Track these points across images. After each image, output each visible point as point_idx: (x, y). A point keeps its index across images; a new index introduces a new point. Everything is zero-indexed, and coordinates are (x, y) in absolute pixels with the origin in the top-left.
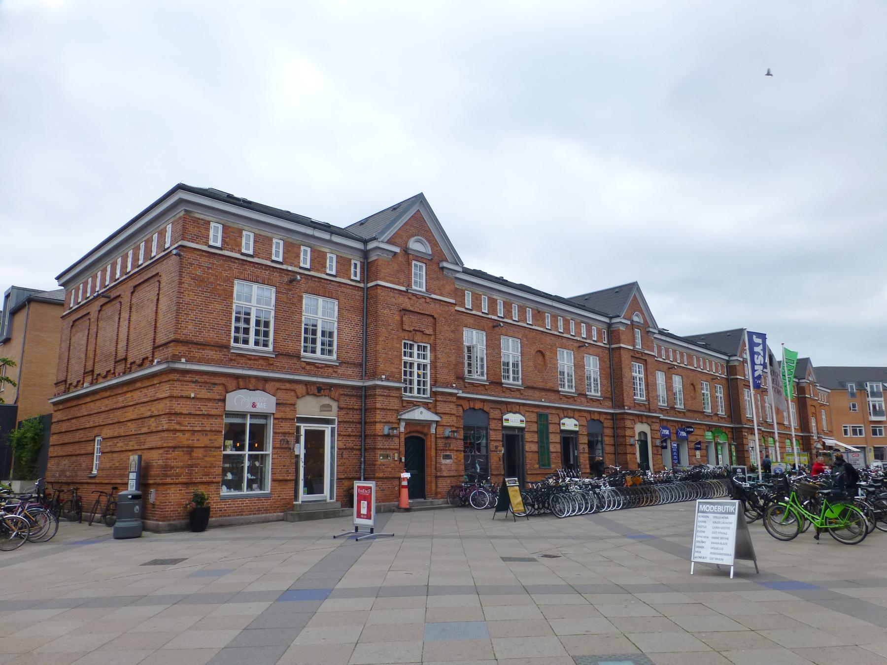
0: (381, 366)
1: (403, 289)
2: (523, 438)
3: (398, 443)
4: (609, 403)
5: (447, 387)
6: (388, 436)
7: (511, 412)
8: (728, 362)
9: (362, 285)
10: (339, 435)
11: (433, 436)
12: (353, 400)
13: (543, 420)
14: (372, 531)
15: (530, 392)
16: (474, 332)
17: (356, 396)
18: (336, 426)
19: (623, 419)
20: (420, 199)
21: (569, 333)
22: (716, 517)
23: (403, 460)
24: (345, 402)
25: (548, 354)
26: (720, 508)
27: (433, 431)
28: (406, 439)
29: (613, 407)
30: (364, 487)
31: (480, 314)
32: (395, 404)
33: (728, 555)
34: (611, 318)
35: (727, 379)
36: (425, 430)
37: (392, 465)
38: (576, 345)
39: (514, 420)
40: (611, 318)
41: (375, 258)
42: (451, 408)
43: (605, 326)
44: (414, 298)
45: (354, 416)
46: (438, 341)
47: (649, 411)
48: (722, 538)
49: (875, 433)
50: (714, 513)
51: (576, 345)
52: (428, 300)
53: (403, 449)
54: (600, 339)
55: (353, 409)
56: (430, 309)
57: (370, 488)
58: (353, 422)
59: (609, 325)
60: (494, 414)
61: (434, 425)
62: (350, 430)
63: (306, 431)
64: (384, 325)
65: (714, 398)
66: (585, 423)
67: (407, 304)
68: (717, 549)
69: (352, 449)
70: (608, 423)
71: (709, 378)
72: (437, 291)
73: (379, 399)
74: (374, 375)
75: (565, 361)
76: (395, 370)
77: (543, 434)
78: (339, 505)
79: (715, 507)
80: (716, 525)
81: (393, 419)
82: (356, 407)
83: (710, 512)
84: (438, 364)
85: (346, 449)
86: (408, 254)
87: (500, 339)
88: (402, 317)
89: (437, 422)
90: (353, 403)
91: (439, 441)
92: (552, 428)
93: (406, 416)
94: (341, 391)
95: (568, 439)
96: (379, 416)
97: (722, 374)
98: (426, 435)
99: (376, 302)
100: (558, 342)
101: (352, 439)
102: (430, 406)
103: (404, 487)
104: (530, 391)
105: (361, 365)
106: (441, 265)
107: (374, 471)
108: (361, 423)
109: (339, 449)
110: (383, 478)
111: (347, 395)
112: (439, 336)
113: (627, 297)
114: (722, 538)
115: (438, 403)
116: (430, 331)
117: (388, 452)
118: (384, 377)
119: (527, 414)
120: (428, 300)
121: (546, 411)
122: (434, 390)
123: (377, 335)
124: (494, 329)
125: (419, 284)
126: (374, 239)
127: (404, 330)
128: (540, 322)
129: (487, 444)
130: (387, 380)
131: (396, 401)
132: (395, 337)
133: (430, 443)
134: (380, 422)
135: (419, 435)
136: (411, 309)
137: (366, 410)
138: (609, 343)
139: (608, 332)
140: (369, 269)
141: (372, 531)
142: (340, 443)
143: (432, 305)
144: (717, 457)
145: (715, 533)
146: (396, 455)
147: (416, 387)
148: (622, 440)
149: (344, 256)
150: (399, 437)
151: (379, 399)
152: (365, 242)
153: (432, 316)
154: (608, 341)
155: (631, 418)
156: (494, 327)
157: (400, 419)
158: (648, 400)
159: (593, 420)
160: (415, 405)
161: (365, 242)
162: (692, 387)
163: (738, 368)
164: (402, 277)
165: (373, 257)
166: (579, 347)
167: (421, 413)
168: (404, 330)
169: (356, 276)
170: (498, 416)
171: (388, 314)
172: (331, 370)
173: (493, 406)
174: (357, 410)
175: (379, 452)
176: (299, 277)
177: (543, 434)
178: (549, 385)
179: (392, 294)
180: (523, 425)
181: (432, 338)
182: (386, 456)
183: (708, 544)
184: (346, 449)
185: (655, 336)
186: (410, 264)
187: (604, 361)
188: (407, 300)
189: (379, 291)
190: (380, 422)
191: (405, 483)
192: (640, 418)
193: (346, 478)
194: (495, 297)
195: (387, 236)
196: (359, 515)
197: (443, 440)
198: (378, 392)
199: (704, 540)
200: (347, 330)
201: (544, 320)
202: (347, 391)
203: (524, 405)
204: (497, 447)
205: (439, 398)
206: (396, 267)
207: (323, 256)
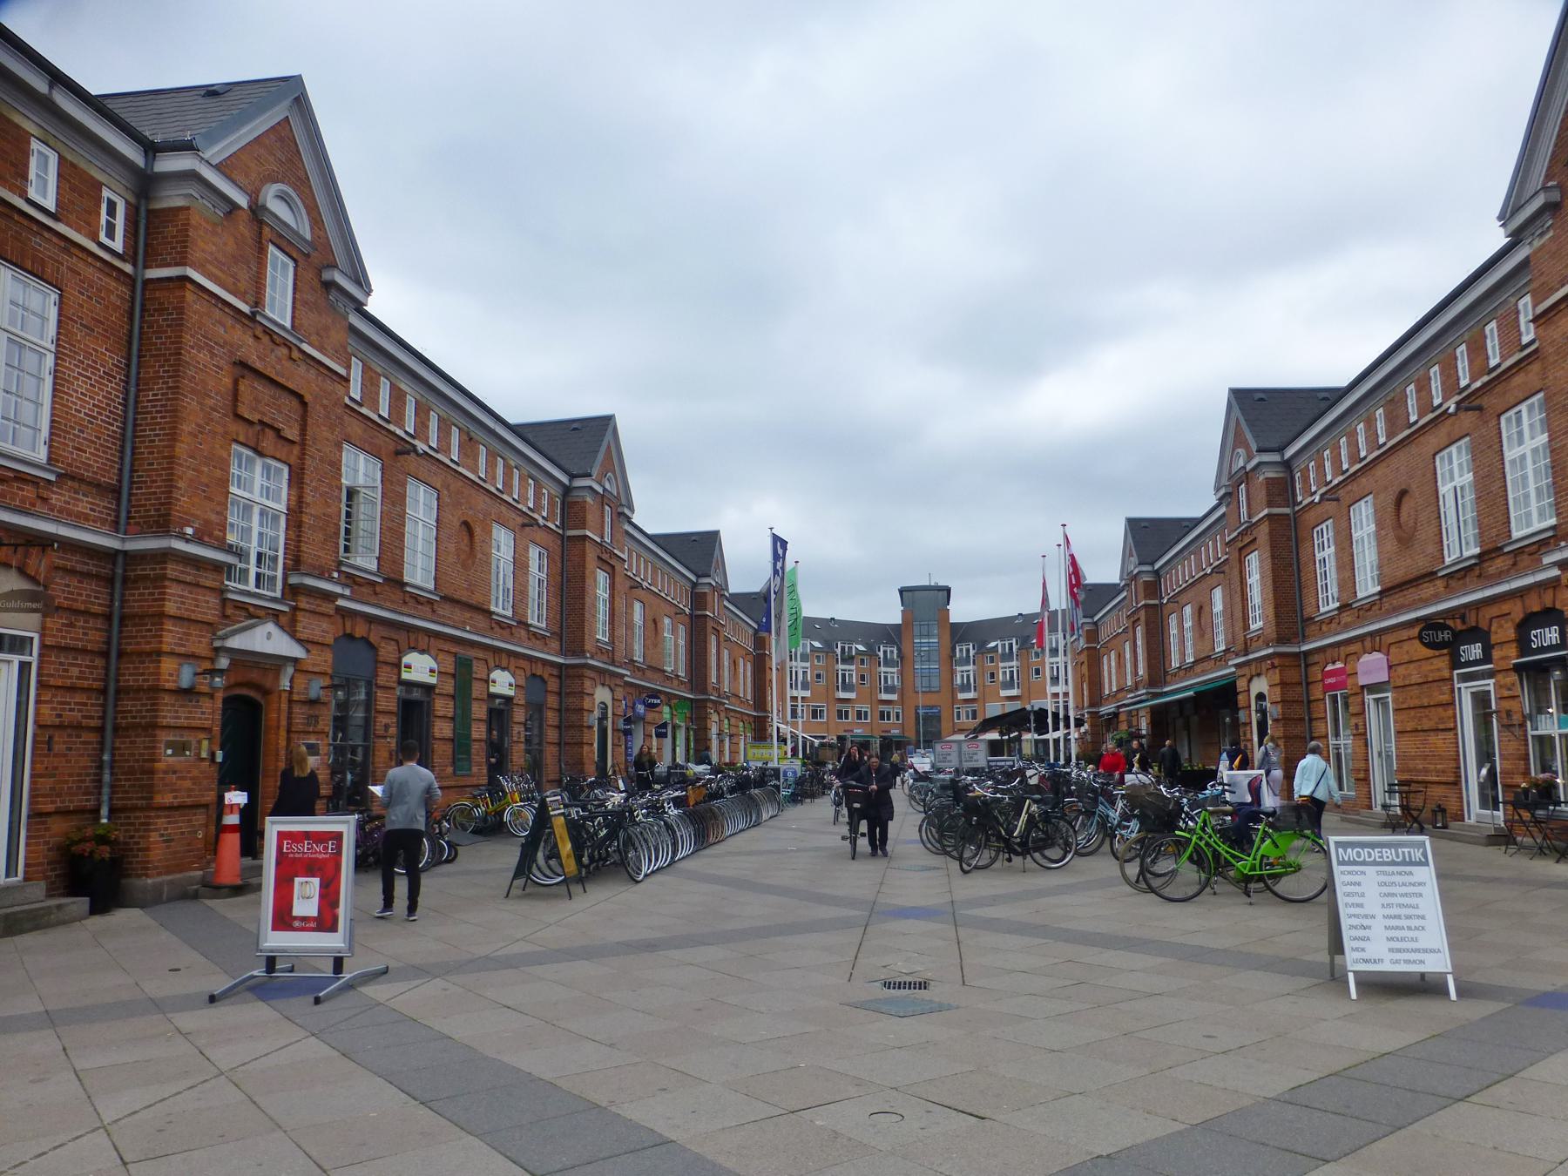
0: (182, 500)
1: (245, 308)
2: (430, 704)
3: (209, 713)
4: (555, 645)
5: (320, 577)
6: (189, 693)
7: (413, 649)
8: (694, 585)
9: (128, 268)
10: (41, 685)
11: (285, 696)
12: (89, 587)
13: (463, 675)
14: (338, 964)
15: (445, 610)
16: (362, 457)
17: (97, 577)
18: (34, 659)
19: (581, 677)
20: (291, 91)
22: (1385, 873)
23: (219, 759)
24: (63, 589)
25: (478, 530)
26: (1388, 854)
27: (285, 684)
28: (226, 701)
29: (561, 653)
30: (307, 835)
31: (375, 418)
32: (208, 607)
33: (1432, 951)
34: (572, 477)
36: (268, 683)
37: (195, 773)
38: (520, 520)
39: (420, 667)
40: (572, 477)
41: (179, 203)
42: (323, 630)
44: (266, 339)
45: (89, 634)
46: (308, 461)
47: (613, 663)
48: (1408, 917)
49: (815, 716)
50: (1375, 863)
51: (520, 520)
52: (295, 355)
53: (217, 729)
55: (86, 613)
56: (301, 378)
57: (338, 837)
58: (84, 651)
59: (567, 490)
60: (387, 651)
61: (290, 670)
62: (75, 671)
64: (193, 391)
66: (522, 682)
67: (251, 352)
68: (1402, 939)
69: (78, 727)
70: (553, 685)
71: (673, 610)
72: (314, 338)
73: (173, 589)
74: (162, 524)
76: (213, 517)
77: (462, 696)
78: (38, 889)
79: (1376, 853)
80: (1386, 890)
81: (202, 649)
82: (96, 609)
83: (1364, 863)
84: (305, 519)
85: (60, 727)
86: (261, 223)
87: (404, 485)
88: (236, 383)
89: (295, 660)
90: (90, 595)
91: (297, 709)
92: (477, 690)
93: (235, 643)
94: (56, 558)
95: (499, 712)
96: (171, 637)
98: (266, 692)
99: (179, 325)
100: (496, 508)
101: (79, 698)
102: (283, 620)
103: (232, 828)
104: (447, 606)
105: (116, 491)
106: (326, 276)
107: (150, 790)
108: (105, 654)
109: (39, 725)
110: (171, 808)
111: (72, 572)
112: (311, 450)
114: (1408, 917)
115: (300, 616)
116: (292, 433)
117: (186, 737)
118: (189, 531)
119: (441, 656)
120: (295, 355)
121: (471, 653)
122: (293, 580)
123: (174, 415)
124: (397, 455)
125: (279, 307)
126: (188, 147)
127: (238, 416)
128: (469, 461)
129: (367, 720)
130: (198, 539)
131: (213, 600)
132: (220, 429)
133: (275, 715)
134: (172, 654)
135: (252, 694)
136: (259, 365)
137: (122, 619)
138: (563, 526)
139: (563, 504)
140: (154, 230)
141: (338, 964)
142: (45, 709)
143: (302, 369)
144: (674, 750)
145: (1389, 906)
146: (205, 744)
147: (253, 570)
148: (574, 717)
149: (82, 165)
150: (212, 696)
151: (173, 589)
152: (152, 150)
153: (300, 397)
154: (562, 522)
155: (592, 674)
156: (398, 453)
157: (217, 650)
158: (612, 642)
159: (533, 678)
160: (253, 614)
161: (152, 150)
162: (463, 539)
163: (709, 598)
164: (244, 276)
165: (172, 198)
166: (524, 525)
167: (269, 636)
168: (238, 416)
169: (111, 234)
170: (392, 658)
171: (205, 368)
172: (29, 492)
173: (385, 634)
174: (95, 615)
175: (166, 737)
177: (462, 696)
178: (475, 599)
179: (217, 314)
180: (433, 680)
181: (296, 450)
182: (180, 748)
183: (1378, 929)
184: (60, 727)
186: (262, 250)
187: (554, 561)
188: (251, 341)
189: (190, 296)
190: (172, 654)
191: (232, 819)
192: (604, 676)
193: (58, 812)
194: (403, 386)
195: (217, 151)
196: (284, 919)
197: (305, 709)
198: (172, 570)
199: (1366, 922)
200: (81, 386)
201: (476, 460)
202: (73, 561)
203: (438, 635)
204: (387, 726)
205: (303, 603)
206: (231, 247)
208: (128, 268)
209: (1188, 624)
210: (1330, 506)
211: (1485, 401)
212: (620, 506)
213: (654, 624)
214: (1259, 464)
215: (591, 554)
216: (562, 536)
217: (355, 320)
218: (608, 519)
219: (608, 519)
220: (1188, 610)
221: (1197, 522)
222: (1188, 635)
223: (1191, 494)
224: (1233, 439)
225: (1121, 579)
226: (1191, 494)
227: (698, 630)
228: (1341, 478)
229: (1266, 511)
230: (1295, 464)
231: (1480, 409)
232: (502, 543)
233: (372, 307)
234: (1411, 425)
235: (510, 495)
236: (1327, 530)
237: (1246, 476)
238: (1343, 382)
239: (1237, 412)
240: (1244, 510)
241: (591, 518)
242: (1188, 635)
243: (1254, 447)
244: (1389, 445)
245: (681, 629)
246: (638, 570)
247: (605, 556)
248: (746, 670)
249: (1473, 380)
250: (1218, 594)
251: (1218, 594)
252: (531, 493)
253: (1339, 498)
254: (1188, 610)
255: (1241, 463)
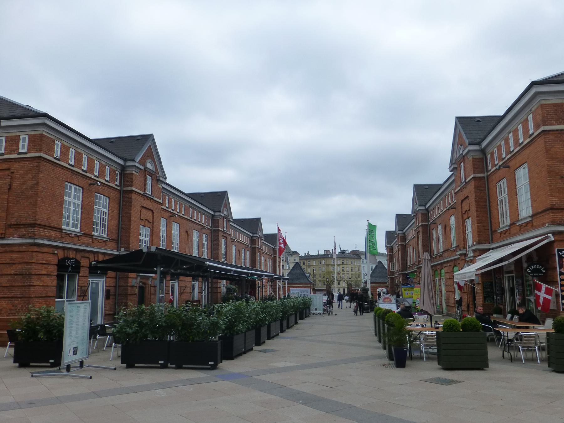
1: (142, 193)
4: (113, 245)
9: (119, 188)
21: (93, 174)
35: (211, 230)
43: (211, 216)
54: (112, 179)
59: (123, 168)
63: (545, 293)
65: (201, 244)
75: (73, 198)
97: (248, 242)
113: (140, 147)
139: (121, 174)
153: (152, 211)
154: (120, 182)
162: (186, 235)
176: (99, 184)
185: (231, 223)
207: (81, 154)
208: (119, 188)
209: (440, 232)
210: (504, 171)
211: (510, 164)
212: (158, 176)
213: (239, 252)
214: (469, 151)
215: (221, 234)
216: (120, 191)
217: (164, 186)
218: (225, 223)
219: (225, 223)
220: (440, 227)
221: (500, 119)
222: (441, 237)
223: (439, 173)
224: (457, 142)
225: (412, 213)
226: (439, 173)
227: (253, 252)
228: (528, 140)
229: (472, 176)
230: (489, 150)
231: (509, 167)
232: (196, 235)
233: (168, 181)
234: (496, 165)
235: (171, 208)
236: (504, 183)
237: (463, 158)
238: (501, 113)
239: (460, 127)
240: (463, 176)
241: (135, 182)
242: (441, 237)
243: (467, 142)
244: (535, 134)
245: (248, 253)
246: (197, 217)
247: (225, 235)
248: (270, 263)
249: (515, 148)
250: (453, 219)
251: (453, 219)
252: (167, 201)
253: (509, 167)
254: (440, 227)
255: (461, 152)
